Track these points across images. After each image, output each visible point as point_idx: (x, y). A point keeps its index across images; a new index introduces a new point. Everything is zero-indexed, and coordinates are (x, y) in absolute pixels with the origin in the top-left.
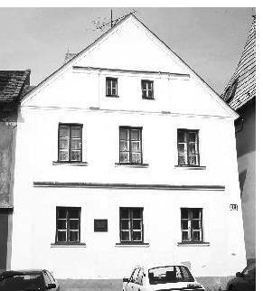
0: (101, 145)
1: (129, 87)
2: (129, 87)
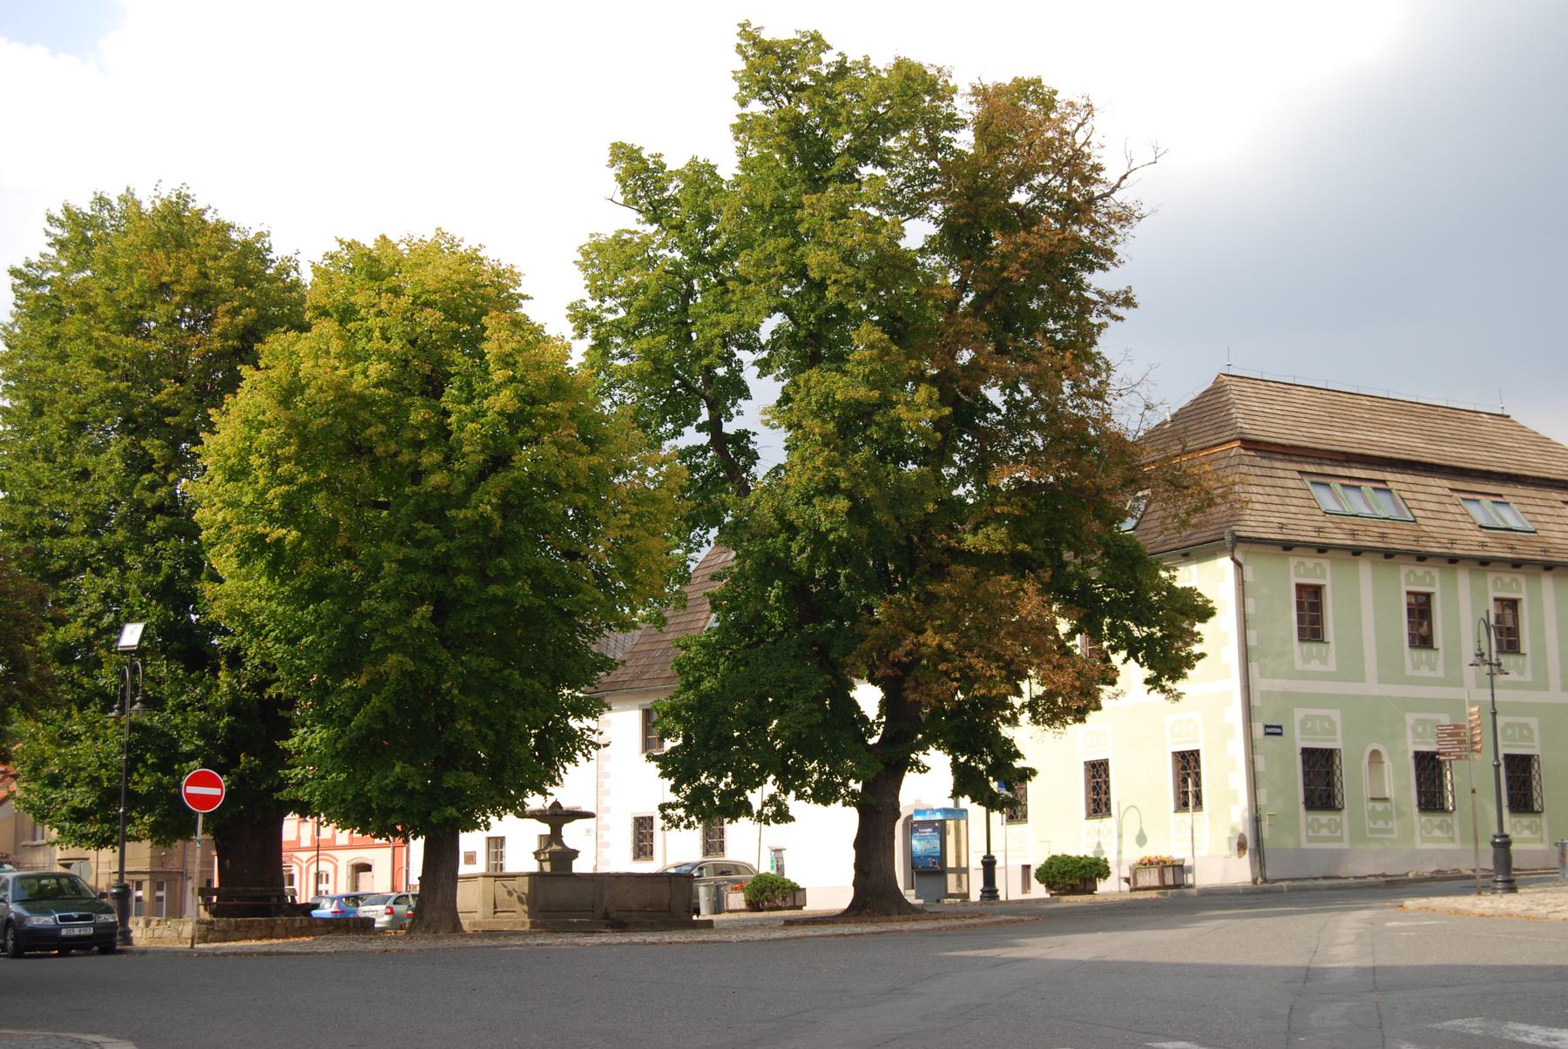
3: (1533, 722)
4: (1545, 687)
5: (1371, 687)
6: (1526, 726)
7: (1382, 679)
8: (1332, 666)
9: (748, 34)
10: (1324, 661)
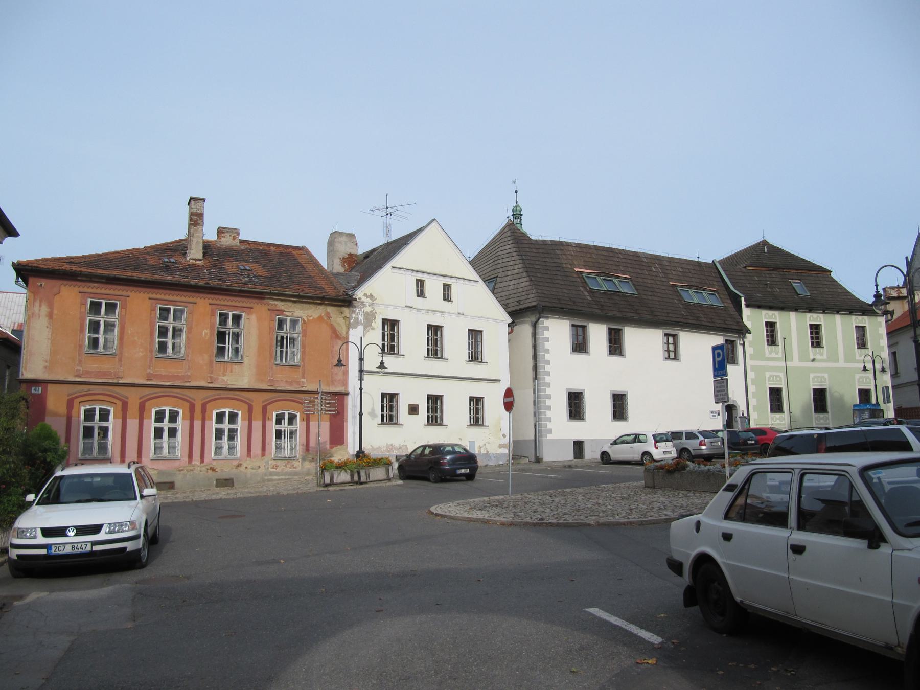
0: (412, 339)
1: (434, 287)
2: (434, 287)
3: (826, 376)
4: (837, 361)
5: (842, 364)
6: (779, 376)
7: (800, 360)
8: (825, 357)
9: (13, 264)
10: (822, 355)
